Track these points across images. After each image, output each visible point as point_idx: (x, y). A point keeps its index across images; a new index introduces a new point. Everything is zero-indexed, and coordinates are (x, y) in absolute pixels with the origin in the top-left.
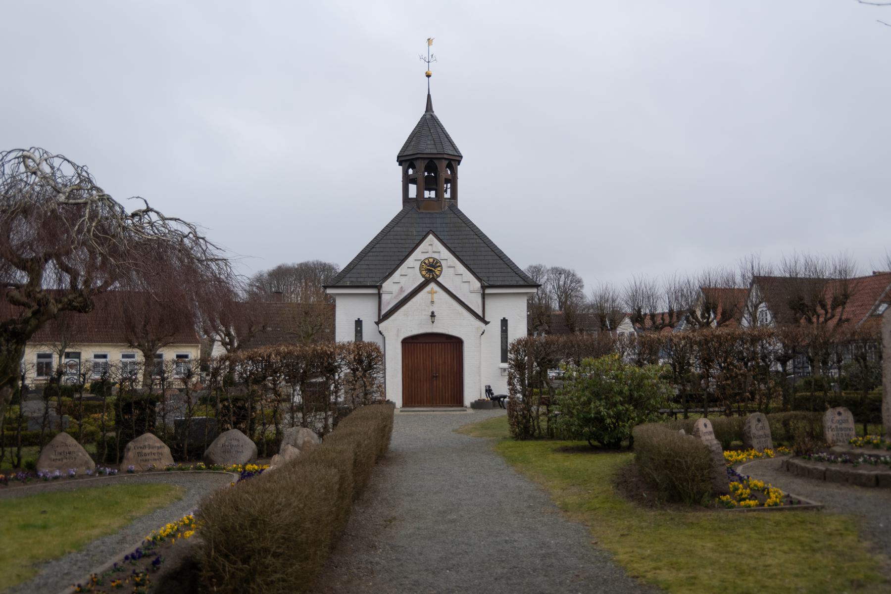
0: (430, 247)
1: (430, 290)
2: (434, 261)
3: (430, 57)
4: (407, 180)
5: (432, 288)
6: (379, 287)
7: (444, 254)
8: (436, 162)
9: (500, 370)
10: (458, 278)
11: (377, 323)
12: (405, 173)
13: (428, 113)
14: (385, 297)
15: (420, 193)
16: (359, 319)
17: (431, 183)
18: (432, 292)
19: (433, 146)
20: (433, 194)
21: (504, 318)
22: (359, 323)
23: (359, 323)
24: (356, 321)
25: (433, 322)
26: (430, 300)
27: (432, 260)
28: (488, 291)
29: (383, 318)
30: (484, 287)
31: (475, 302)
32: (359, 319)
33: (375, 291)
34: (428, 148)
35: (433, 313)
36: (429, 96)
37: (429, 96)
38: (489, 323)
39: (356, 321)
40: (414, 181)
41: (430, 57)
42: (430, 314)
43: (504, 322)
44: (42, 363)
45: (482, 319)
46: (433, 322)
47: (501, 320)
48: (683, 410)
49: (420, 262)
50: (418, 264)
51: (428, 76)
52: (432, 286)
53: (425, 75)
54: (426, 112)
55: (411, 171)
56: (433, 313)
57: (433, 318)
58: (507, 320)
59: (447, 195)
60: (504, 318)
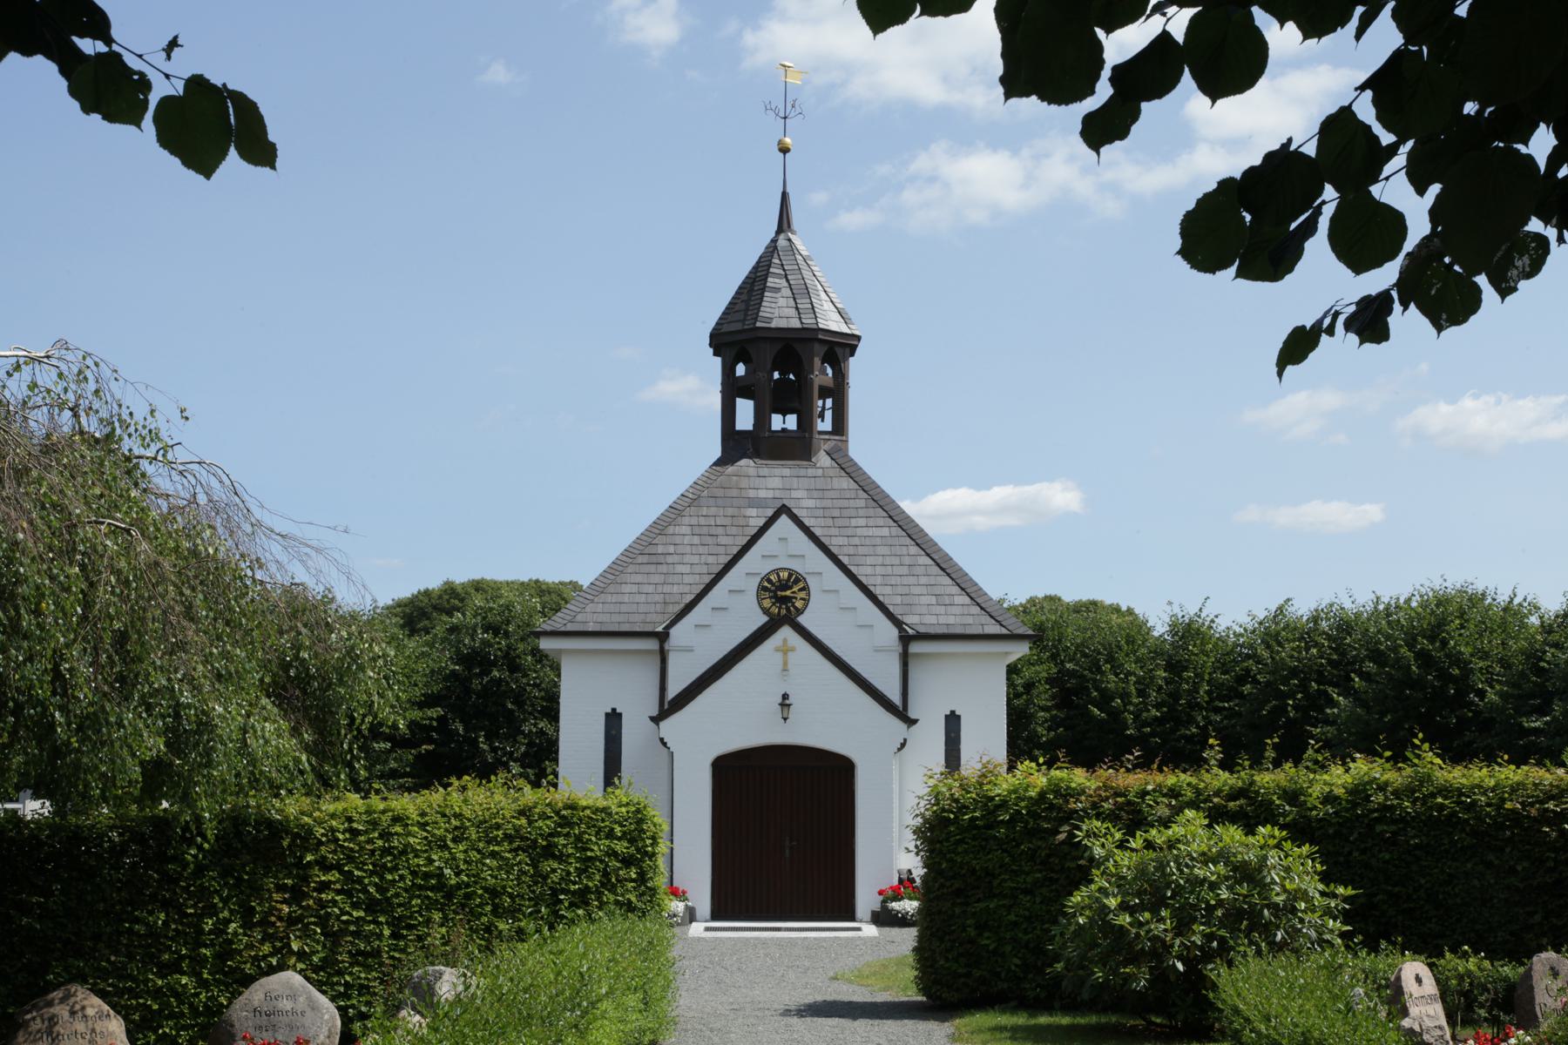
2: (790, 575)
4: (732, 390)
5: (785, 641)
6: (663, 637)
7: (812, 563)
11: (656, 720)
12: (728, 371)
14: (673, 661)
15: (761, 418)
17: (792, 397)
18: (785, 650)
19: (793, 312)
20: (791, 422)
21: (953, 712)
22: (613, 720)
23: (613, 720)
24: (607, 714)
25: (785, 719)
27: (786, 574)
28: (915, 648)
29: (669, 707)
30: (906, 639)
31: (889, 685)
33: (652, 645)
34: (778, 312)
36: (784, 196)
37: (784, 196)
39: (607, 714)
43: (953, 721)
45: (901, 713)
46: (785, 719)
51: (784, 150)
52: (786, 632)
53: (776, 149)
55: (741, 370)
57: (786, 709)
59: (825, 425)
60: (953, 712)
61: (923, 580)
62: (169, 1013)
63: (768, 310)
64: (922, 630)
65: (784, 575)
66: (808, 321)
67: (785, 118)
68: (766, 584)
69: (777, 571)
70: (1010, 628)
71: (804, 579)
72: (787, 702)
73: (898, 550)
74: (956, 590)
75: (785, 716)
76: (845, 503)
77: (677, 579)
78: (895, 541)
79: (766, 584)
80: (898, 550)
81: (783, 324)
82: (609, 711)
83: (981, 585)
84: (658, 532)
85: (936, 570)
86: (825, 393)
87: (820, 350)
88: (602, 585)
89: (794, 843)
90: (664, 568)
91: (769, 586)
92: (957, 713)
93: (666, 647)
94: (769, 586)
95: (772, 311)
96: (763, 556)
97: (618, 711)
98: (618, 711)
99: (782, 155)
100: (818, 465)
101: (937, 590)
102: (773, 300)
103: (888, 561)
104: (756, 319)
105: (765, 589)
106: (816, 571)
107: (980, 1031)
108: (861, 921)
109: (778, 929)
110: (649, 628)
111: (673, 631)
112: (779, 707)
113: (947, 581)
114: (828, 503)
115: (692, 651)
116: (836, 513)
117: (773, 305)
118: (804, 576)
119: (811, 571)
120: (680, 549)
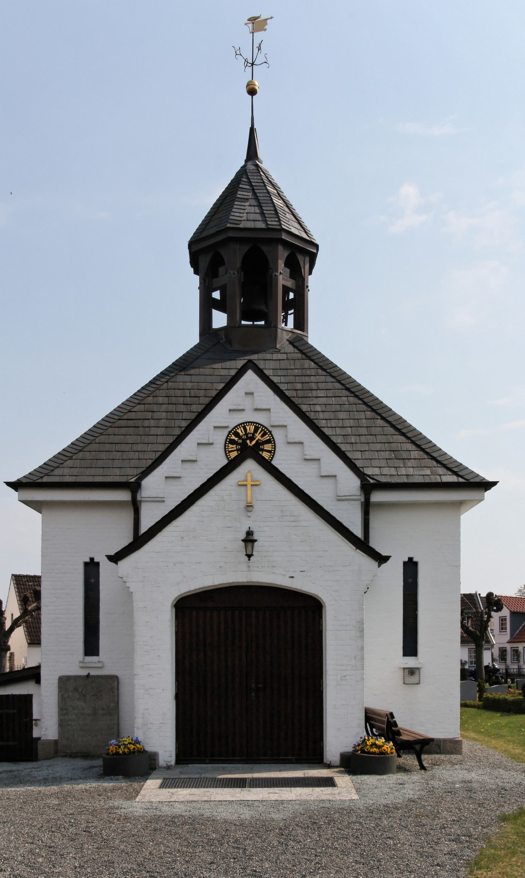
0: (249, 398)
1: (242, 478)
3: (256, 50)
8: (265, 248)
9: (401, 673)
10: (312, 467)
13: (249, 163)
16: (92, 559)
19: (258, 217)
21: (411, 559)
24: (86, 564)
25: (249, 556)
26: (243, 504)
27: (252, 428)
28: (377, 497)
32: (92, 559)
33: (124, 496)
35: (249, 533)
36: (252, 131)
37: (252, 131)
38: (386, 559)
39: (86, 564)
40: (221, 306)
41: (256, 50)
42: (243, 536)
44: (505, 630)
46: (249, 556)
47: (405, 563)
48: (194, 614)
49: (226, 432)
50: (220, 438)
51: (252, 92)
54: (246, 161)
56: (249, 533)
57: (249, 545)
58: (416, 564)
60: (411, 559)
61: (380, 438)
62: (495, 678)
63: (236, 214)
64: (383, 480)
65: (251, 429)
66: (273, 223)
67: (253, 64)
68: (233, 437)
69: (243, 425)
70: (466, 477)
71: (270, 432)
72: (251, 538)
73: (357, 415)
74: (411, 447)
75: (249, 553)
76: (306, 379)
77: (152, 439)
78: (354, 408)
79: (233, 437)
80: (357, 415)
81: (250, 225)
82: (88, 560)
83: (434, 441)
84: (137, 401)
85: (391, 430)
86: (287, 305)
87: (283, 254)
88: (82, 445)
89: (261, 686)
90: (141, 431)
91: (236, 439)
92: (415, 560)
93: (139, 498)
94: (236, 439)
95: (241, 215)
96: (230, 410)
97: (96, 560)
98: (96, 560)
99: (251, 97)
100: (282, 351)
101: (394, 446)
102: (243, 207)
103: (347, 423)
104: (227, 222)
105: (232, 442)
106: (280, 424)
107: (334, 772)
108: (329, 766)
109: (241, 783)
110: (123, 479)
111: (145, 482)
112: (243, 544)
113: (402, 438)
114: (292, 379)
115: (163, 501)
116: (299, 386)
117: (242, 211)
118: (270, 429)
119: (276, 424)
120: (156, 415)
